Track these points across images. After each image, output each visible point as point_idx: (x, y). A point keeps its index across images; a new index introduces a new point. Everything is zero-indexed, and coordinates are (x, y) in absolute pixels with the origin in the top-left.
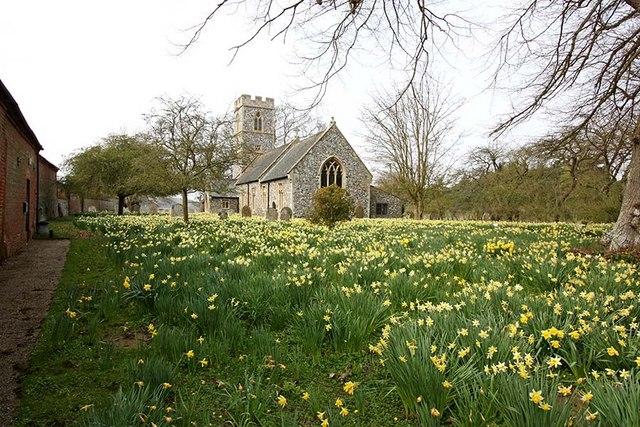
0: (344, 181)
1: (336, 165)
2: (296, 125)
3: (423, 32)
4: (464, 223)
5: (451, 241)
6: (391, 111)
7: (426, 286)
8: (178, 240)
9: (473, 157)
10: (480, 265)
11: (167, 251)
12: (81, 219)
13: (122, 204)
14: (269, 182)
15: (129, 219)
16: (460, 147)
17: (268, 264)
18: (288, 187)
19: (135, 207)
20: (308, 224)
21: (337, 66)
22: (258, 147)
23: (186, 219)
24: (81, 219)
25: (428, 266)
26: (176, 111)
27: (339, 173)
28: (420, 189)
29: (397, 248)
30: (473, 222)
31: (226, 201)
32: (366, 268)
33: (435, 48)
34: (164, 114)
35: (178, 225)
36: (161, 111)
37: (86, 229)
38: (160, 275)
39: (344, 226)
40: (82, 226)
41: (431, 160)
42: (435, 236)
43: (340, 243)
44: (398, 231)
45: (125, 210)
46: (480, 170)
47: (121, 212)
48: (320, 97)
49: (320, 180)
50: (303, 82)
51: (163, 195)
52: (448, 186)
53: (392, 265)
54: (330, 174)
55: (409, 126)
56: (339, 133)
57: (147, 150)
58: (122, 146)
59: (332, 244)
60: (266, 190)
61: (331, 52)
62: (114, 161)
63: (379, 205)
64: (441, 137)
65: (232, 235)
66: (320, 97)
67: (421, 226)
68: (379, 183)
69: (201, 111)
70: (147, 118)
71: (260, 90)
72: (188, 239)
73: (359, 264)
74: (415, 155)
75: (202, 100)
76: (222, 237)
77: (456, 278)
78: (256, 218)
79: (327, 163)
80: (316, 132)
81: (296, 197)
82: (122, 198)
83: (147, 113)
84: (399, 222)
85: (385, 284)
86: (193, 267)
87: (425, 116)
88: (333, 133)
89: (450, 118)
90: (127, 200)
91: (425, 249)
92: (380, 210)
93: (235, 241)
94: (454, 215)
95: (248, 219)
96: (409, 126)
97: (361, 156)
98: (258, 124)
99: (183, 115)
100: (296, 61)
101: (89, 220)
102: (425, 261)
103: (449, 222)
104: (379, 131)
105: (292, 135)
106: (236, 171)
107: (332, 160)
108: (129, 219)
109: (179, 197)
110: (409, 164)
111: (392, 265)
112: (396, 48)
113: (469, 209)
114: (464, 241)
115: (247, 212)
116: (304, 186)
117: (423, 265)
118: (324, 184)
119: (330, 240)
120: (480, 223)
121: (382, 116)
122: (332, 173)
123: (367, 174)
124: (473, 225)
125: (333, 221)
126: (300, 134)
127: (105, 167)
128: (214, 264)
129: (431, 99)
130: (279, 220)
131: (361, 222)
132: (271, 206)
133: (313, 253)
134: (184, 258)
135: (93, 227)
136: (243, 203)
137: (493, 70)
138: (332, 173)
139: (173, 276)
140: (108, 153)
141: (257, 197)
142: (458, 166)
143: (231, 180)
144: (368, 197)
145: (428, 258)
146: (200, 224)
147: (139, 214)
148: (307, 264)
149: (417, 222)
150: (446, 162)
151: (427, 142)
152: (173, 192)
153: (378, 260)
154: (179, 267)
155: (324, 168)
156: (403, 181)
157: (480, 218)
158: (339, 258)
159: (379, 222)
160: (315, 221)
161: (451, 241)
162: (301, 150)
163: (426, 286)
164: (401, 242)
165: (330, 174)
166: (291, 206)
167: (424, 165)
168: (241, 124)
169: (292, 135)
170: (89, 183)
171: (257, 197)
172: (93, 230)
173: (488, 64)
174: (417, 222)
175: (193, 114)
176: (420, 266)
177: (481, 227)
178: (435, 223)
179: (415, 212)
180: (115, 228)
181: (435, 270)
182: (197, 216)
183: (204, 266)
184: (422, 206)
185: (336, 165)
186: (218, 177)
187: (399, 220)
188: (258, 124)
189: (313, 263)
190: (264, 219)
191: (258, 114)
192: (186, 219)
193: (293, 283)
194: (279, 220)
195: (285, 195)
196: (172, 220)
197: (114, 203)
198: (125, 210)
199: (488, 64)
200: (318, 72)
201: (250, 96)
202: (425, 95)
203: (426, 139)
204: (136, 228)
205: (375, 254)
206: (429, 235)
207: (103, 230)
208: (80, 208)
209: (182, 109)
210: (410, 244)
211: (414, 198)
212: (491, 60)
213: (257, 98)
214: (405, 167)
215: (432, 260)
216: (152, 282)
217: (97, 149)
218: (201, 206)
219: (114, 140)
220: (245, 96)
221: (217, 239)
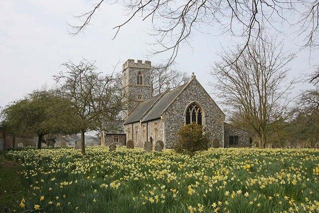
0: (203, 120)
1: (196, 108)
2: (168, 79)
3: (254, 7)
4: (299, 150)
5: (286, 166)
6: (233, 64)
7: (259, 205)
8: (74, 167)
9: (304, 98)
10: (309, 186)
11: (63, 176)
12: (10, 153)
13: (41, 140)
14: (147, 122)
15: (45, 152)
16: (292, 91)
17: (137, 186)
18: (162, 126)
19: (51, 143)
20: (174, 153)
21: (185, 34)
22: (140, 97)
23: (83, 151)
24: (10, 153)
25: (263, 186)
26: (77, 73)
27: (200, 114)
28: (264, 124)
29: (240, 173)
30: (307, 149)
31: (116, 137)
32: (210, 190)
33: (264, 18)
34: (68, 75)
35: (77, 156)
36: (67, 74)
37: (13, 160)
38: (50, 196)
39: (200, 154)
40: (10, 158)
41: (270, 102)
42: (273, 162)
43: (196, 169)
44: (242, 158)
45: (43, 145)
46: (311, 108)
47: (39, 147)
48: (173, 58)
49: (185, 120)
50: (159, 48)
51: (70, 134)
52: (286, 121)
53: (233, 186)
54: (193, 115)
55: (251, 76)
56: (198, 84)
57: (57, 100)
58: (42, 99)
59: (189, 170)
60: (145, 128)
61: (181, 25)
62: (35, 110)
63: (231, 138)
64: (277, 83)
65: (115, 163)
66: (173, 58)
67: (262, 154)
68: (232, 120)
69: (96, 71)
70: (57, 79)
71: (138, 56)
72: (81, 167)
73: (207, 186)
74: (257, 99)
75: (95, 64)
76: (106, 165)
77: (286, 197)
78: (137, 150)
79: (190, 107)
80: (183, 83)
81: (167, 133)
82: (41, 136)
83: (57, 75)
84: (246, 151)
85: (227, 203)
86: (77, 189)
87: (260, 68)
88: (193, 84)
89: (283, 70)
90: (45, 137)
91: (262, 173)
92: (232, 141)
93: (116, 167)
94: (293, 144)
95: (131, 150)
96: (251, 76)
97: (215, 100)
98: (139, 80)
99: (82, 75)
100: (152, 33)
101: (14, 154)
102: (260, 183)
103: (286, 150)
104: (228, 82)
105: (165, 86)
106: (122, 115)
107: (194, 104)
108: (45, 152)
109: (79, 135)
110: (253, 106)
111: (233, 186)
112: (235, 18)
113: (305, 139)
114: (297, 166)
115: (131, 145)
116: (173, 124)
117: (259, 186)
118: (188, 122)
119: (189, 166)
120: (312, 150)
121: (228, 69)
122: (194, 114)
123: (221, 114)
124: (307, 152)
125: (194, 151)
126: (172, 86)
127: (30, 114)
128: (96, 186)
129: (267, 56)
130: (154, 150)
131: (217, 151)
132: (149, 140)
133: (172, 177)
134: (71, 183)
135: (17, 158)
136: (129, 138)
137: (308, 32)
138: (194, 114)
139: (61, 198)
140: (31, 104)
141: (139, 134)
142: (292, 105)
143: (121, 121)
144: (223, 132)
145: (264, 181)
146: (93, 156)
147: (53, 148)
148: (164, 186)
149: (261, 150)
150: (281, 102)
151: (266, 89)
152: (76, 132)
153: (220, 183)
154: (66, 189)
155: (188, 110)
156: (248, 118)
157: (313, 146)
158: (192, 181)
159: (231, 151)
160: (179, 151)
161: (286, 166)
162: (171, 97)
163: (259, 205)
164: (245, 167)
165: (193, 115)
166: (164, 140)
167: (264, 106)
168: (127, 80)
169: (165, 86)
170: (17, 127)
171: (139, 134)
172: (17, 161)
173: (305, 28)
174: (261, 150)
175: (89, 75)
176: (257, 187)
177: (311, 154)
178: (275, 151)
179: (259, 141)
180: (32, 158)
181: (268, 191)
182: (91, 149)
183: (88, 188)
184: (265, 138)
185: (196, 108)
186: (112, 119)
187: (247, 148)
188: (139, 80)
189: (170, 186)
190: (142, 150)
191: (140, 73)
192: (83, 151)
193: (148, 202)
194: (154, 150)
195: (159, 132)
196: (75, 152)
197: (36, 139)
198: (43, 145)
199: (305, 28)
200: (170, 41)
201: (134, 60)
202: (262, 54)
203: (264, 85)
204: (47, 158)
205: (218, 178)
206: (267, 161)
207: (23, 161)
208: (12, 145)
209: (82, 71)
210: (251, 169)
211: (258, 131)
212: (307, 24)
213: (139, 61)
214: (249, 108)
215: (266, 182)
216: (42, 203)
217: (24, 102)
218: (98, 140)
219: (36, 95)
220: (130, 61)
221: (102, 166)
